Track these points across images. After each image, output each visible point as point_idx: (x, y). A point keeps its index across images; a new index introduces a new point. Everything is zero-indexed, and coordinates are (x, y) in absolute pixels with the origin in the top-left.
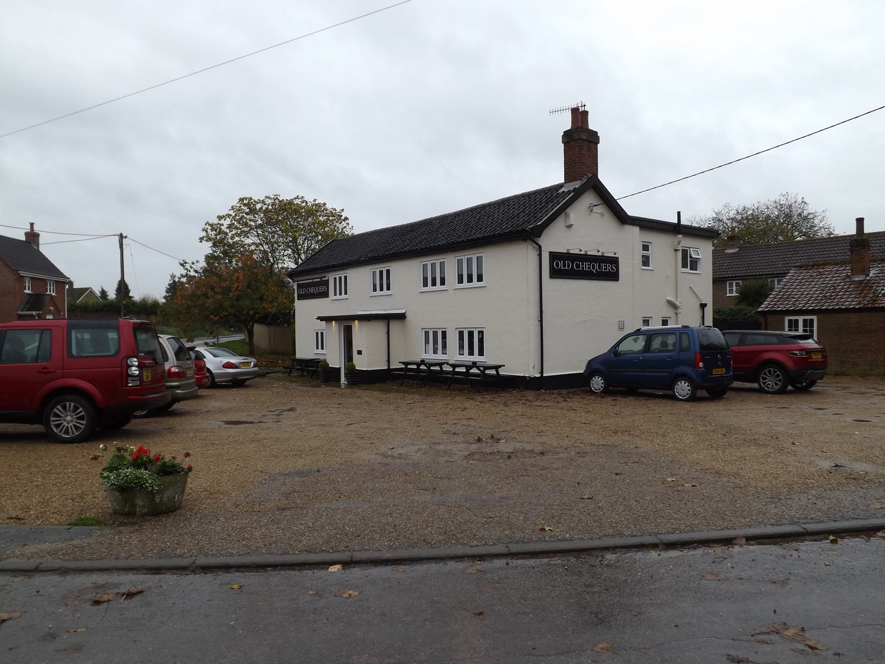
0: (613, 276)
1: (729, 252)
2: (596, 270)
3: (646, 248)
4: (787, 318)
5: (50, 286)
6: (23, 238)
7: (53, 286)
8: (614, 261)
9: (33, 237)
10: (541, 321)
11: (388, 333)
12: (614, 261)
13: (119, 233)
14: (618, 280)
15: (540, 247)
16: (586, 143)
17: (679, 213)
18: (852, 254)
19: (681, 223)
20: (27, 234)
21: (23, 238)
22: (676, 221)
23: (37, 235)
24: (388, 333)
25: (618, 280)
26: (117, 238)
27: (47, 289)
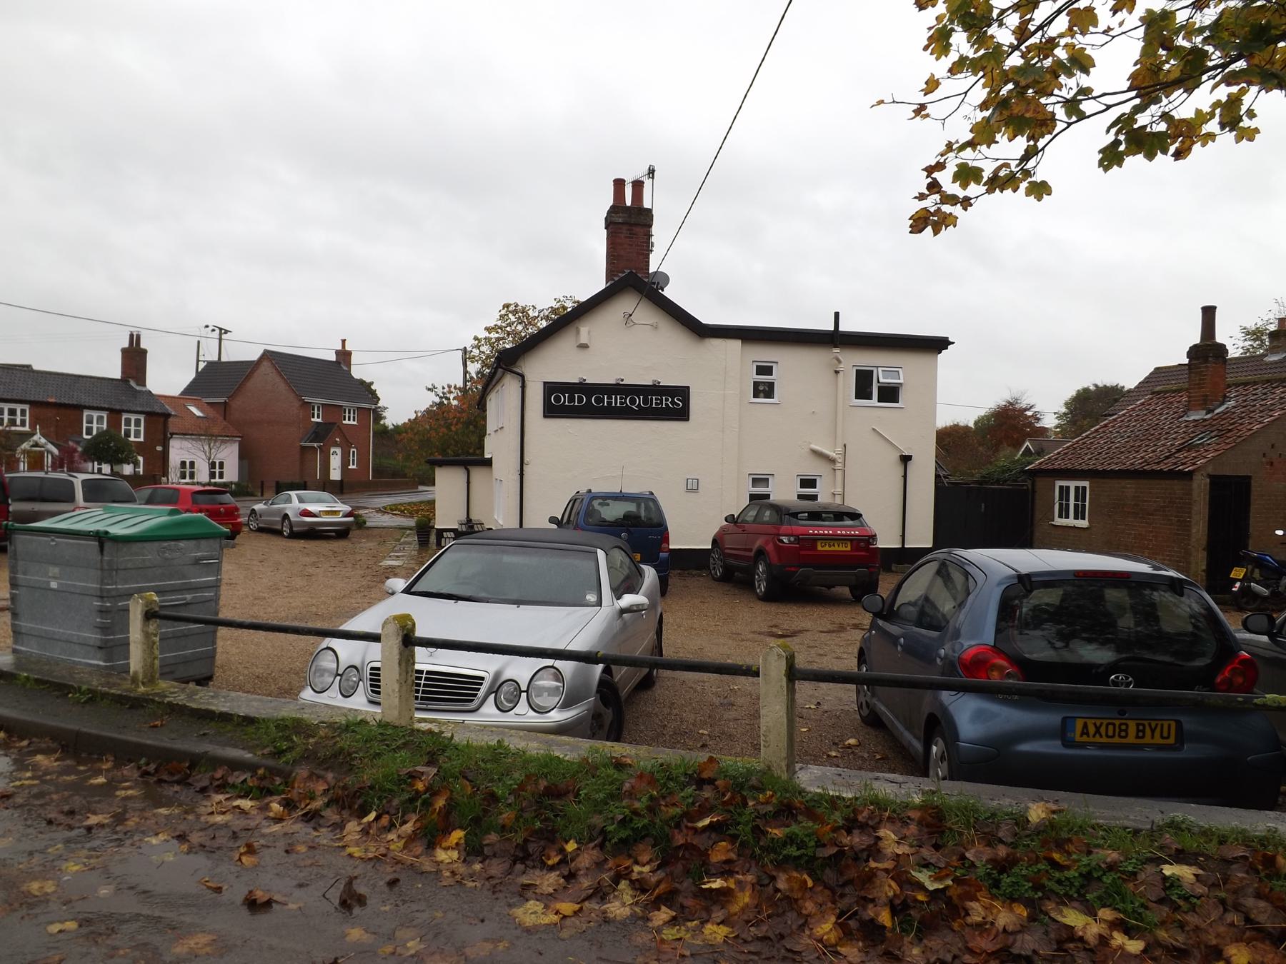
0: (682, 414)
1: (1271, 359)
2: (639, 406)
3: (764, 370)
4: (1059, 483)
5: (349, 413)
6: (334, 359)
7: (354, 414)
8: (683, 393)
9: (344, 356)
10: (522, 475)
11: (468, 483)
12: (683, 393)
13: (462, 347)
14: (687, 419)
15: (522, 376)
16: (625, 228)
17: (837, 315)
18: (1190, 373)
19: (840, 329)
20: (337, 353)
21: (334, 359)
22: (216, 359)
23: (349, 354)
24: (468, 483)
25: (687, 419)
26: (460, 353)
27: (345, 417)
